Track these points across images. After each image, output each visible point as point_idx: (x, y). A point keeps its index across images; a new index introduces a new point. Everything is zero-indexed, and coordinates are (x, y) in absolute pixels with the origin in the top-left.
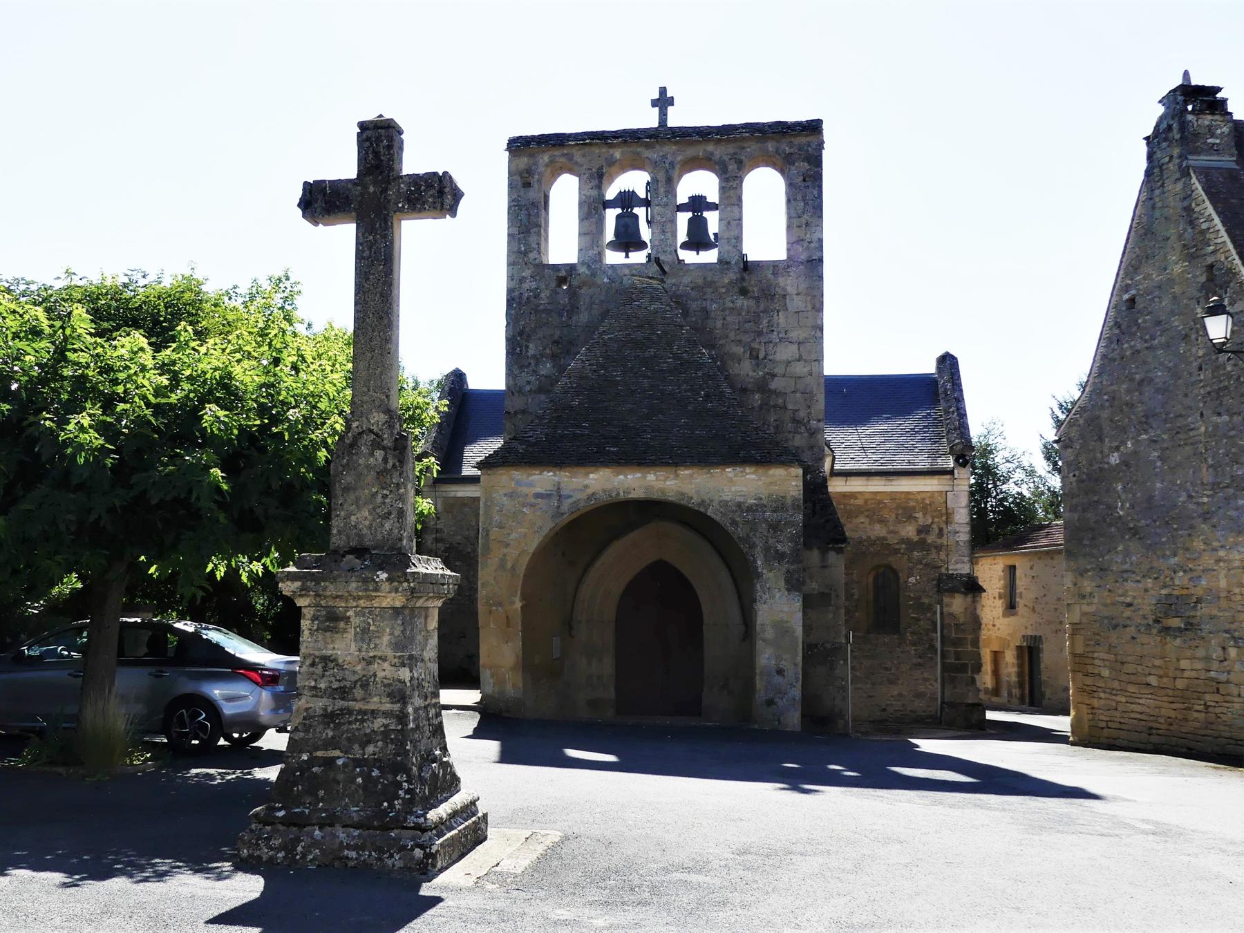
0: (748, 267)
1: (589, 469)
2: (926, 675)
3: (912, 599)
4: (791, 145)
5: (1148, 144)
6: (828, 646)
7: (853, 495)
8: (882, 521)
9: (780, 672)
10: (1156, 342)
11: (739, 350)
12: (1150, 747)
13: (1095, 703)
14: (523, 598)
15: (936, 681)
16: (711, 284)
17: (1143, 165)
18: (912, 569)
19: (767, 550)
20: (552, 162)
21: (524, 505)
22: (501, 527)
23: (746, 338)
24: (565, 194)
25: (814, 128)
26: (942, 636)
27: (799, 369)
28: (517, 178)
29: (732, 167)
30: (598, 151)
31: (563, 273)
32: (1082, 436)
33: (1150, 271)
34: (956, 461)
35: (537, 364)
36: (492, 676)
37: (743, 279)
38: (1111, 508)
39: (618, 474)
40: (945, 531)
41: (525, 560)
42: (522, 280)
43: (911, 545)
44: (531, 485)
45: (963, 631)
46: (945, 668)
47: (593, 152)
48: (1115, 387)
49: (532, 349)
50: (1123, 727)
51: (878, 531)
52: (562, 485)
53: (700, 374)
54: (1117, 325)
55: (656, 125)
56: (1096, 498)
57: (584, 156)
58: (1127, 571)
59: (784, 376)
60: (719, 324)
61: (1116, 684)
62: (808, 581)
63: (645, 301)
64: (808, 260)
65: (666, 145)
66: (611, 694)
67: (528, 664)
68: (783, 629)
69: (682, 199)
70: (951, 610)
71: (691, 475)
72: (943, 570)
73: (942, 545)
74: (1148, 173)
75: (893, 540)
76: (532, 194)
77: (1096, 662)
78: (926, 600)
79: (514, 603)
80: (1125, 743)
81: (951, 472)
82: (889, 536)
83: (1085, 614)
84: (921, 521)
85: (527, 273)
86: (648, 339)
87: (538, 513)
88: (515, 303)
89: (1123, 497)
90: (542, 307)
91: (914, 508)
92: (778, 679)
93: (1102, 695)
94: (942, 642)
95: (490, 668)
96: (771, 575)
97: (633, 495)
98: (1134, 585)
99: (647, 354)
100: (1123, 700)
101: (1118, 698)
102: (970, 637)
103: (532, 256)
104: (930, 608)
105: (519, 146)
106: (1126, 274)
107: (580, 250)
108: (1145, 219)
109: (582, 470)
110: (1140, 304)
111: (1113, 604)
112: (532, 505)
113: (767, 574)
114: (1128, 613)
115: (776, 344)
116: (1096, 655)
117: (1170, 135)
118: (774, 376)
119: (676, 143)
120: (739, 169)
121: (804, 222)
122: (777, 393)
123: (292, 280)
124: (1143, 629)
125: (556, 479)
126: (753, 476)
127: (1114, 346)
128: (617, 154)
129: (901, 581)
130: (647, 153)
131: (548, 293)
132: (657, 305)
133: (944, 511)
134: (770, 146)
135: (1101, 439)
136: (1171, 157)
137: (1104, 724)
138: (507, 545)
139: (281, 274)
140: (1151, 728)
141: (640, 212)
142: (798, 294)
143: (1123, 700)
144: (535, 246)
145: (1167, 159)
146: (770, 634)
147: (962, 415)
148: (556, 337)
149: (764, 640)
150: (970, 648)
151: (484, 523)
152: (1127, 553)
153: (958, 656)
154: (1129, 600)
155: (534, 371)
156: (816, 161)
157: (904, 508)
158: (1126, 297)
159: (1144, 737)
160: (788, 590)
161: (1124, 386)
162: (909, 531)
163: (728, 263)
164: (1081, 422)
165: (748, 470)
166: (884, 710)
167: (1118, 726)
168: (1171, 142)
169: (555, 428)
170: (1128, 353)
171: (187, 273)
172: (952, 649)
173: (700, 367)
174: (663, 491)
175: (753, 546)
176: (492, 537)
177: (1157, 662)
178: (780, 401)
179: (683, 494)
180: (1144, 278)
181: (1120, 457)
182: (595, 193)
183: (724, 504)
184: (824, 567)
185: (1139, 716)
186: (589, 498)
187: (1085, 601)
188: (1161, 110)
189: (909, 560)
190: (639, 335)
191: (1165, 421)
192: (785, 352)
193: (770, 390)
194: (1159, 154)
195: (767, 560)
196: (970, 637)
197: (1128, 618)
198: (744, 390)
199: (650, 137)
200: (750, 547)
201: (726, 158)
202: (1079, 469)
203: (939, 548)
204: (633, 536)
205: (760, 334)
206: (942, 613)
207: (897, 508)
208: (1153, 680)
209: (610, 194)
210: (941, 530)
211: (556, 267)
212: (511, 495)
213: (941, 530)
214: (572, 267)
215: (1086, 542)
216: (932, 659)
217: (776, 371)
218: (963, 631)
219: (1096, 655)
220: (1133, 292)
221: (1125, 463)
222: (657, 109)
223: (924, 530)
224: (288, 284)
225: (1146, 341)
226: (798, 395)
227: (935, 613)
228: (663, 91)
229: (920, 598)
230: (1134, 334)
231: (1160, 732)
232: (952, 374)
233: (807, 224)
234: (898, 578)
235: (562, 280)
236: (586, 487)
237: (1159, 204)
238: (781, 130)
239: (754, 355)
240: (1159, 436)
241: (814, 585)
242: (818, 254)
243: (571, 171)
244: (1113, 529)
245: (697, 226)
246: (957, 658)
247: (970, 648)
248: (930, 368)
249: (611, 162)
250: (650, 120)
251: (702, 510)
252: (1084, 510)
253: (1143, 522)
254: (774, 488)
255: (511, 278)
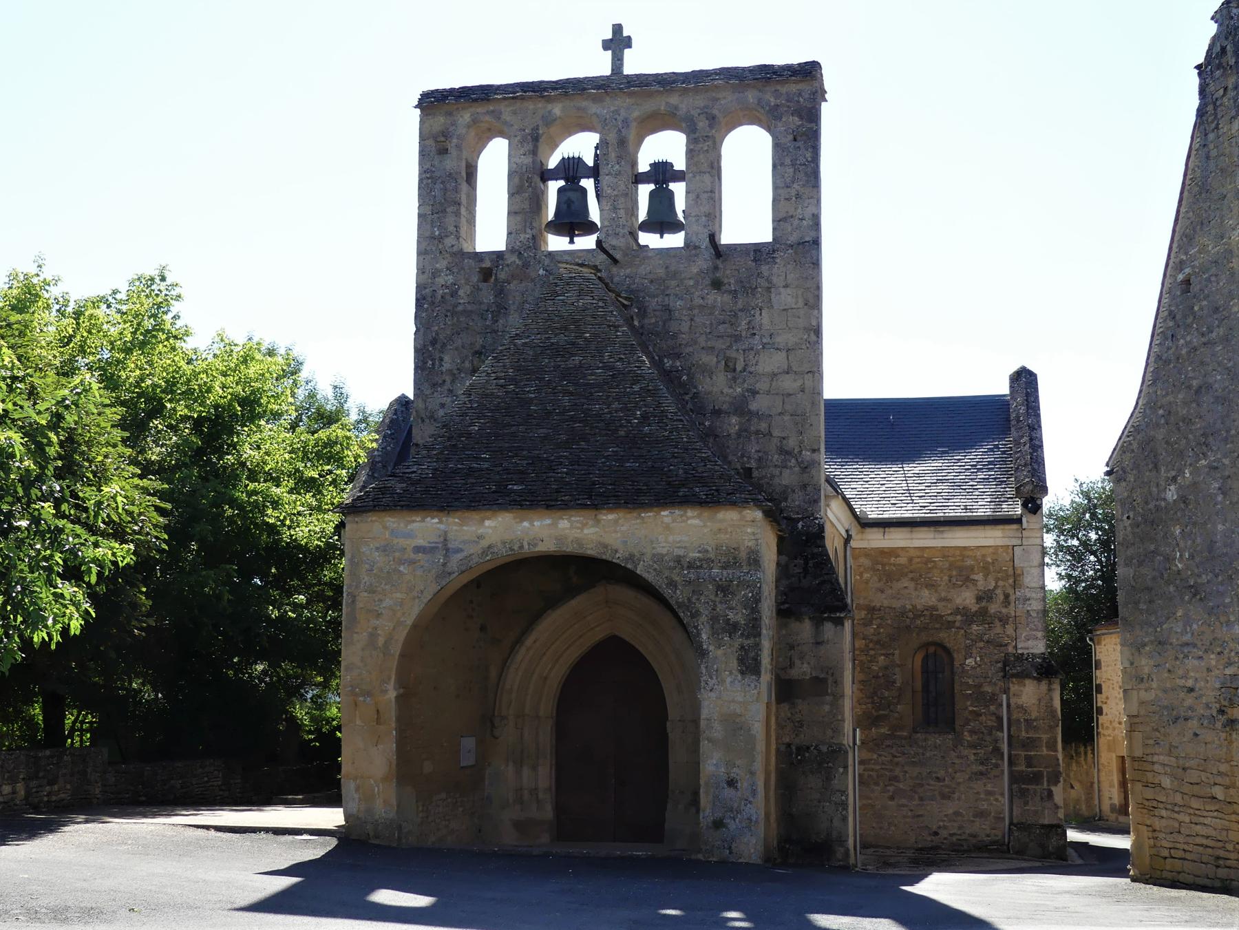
0: (720, 252)
1: (483, 514)
2: (989, 787)
3: (969, 687)
4: (777, 94)
5: (1199, 74)
6: (824, 749)
7: (893, 552)
8: (931, 586)
9: (731, 783)
10: (1214, 335)
11: (709, 359)
12: (1218, 884)
13: (1157, 824)
14: (401, 682)
15: (1002, 794)
16: (674, 275)
17: (1195, 102)
18: (968, 647)
19: (714, 619)
20: (475, 121)
21: (401, 562)
22: (372, 591)
23: (720, 345)
24: (494, 162)
25: (809, 72)
26: (1010, 736)
27: (788, 384)
28: (430, 142)
29: (702, 124)
30: (534, 106)
31: (487, 264)
32: (1136, 466)
33: (1205, 240)
34: (1024, 505)
35: (453, 381)
36: (357, 790)
37: (716, 268)
38: (1169, 559)
39: (522, 521)
40: (1012, 598)
41: (402, 635)
42: (435, 274)
43: (969, 617)
44: (409, 535)
45: (1036, 729)
46: (1015, 778)
47: (528, 108)
48: (1170, 398)
49: (448, 362)
50: (1188, 856)
51: (926, 598)
52: (450, 536)
53: (636, 388)
54: (1172, 315)
55: (607, 71)
56: (1152, 547)
57: (515, 113)
58: (1187, 644)
59: (768, 393)
60: (685, 327)
61: (1178, 798)
62: (798, 662)
63: (571, 296)
64: (797, 241)
65: (625, 98)
66: (548, 813)
67: (406, 769)
68: (735, 725)
69: (643, 167)
70: (1020, 702)
71: (616, 521)
72: (1010, 649)
73: (1008, 617)
74: (1201, 113)
75: (945, 610)
76: (450, 163)
77: (1156, 767)
78: (988, 689)
79: (386, 691)
80: (1190, 879)
81: (1018, 521)
82: (940, 605)
83: (1142, 703)
84: (981, 585)
85: (441, 265)
86: (573, 344)
87: (419, 572)
88: (425, 301)
89: (1182, 544)
90: (460, 308)
91: (972, 569)
92: (728, 792)
93: (1164, 813)
94: (1010, 745)
95: (355, 779)
96: (720, 652)
97: (542, 548)
98: (1196, 662)
99: (570, 364)
100: (1187, 819)
101: (1182, 817)
102: (1045, 737)
103: (449, 241)
104: (993, 699)
105: (432, 102)
106: (1180, 247)
107: (509, 234)
108: (1198, 173)
109: (476, 516)
110: (1195, 288)
111: (1173, 689)
112: (412, 562)
113: (714, 652)
114: (1189, 702)
115: (757, 353)
116: (1155, 758)
117: (1224, 60)
118: (754, 393)
119: (631, 94)
120: (711, 126)
121: (793, 192)
122: (758, 415)
123: (169, 282)
124: (1205, 723)
125: (442, 527)
126: (696, 522)
127: (1168, 343)
128: (557, 109)
129: (957, 664)
130: (594, 108)
131: (468, 289)
132: (588, 300)
133: (1011, 571)
134: (751, 96)
135: (1156, 468)
136: (1226, 89)
137: (1165, 853)
138: (379, 615)
139: (155, 273)
140: (1218, 858)
141: (588, 184)
142: (786, 286)
143: (1187, 819)
144: (451, 228)
145: (1221, 92)
146: (717, 731)
147: (1036, 446)
148: (478, 347)
149: (709, 740)
150: (1045, 751)
151: (350, 586)
152: (1187, 622)
153: (1029, 761)
154: (1190, 683)
155: (450, 391)
156: (812, 116)
157: (961, 569)
158: (1181, 277)
159: (1210, 870)
160: (742, 673)
161: (1180, 396)
162: (966, 598)
163: (696, 247)
164: (1135, 446)
165: (690, 513)
166: (936, 834)
167: (1180, 854)
168: (1225, 69)
169: (447, 460)
170: (1184, 351)
171: (33, 270)
172: (1023, 754)
173: (637, 379)
174: (578, 541)
175: (696, 615)
176: (360, 605)
177: (1224, 768)
178: (763, 426)
179: (606, 546)
180: (1200, 252)
181: (1177, 490)
182: (528, 160)
183: (658, 558)
184: (818, 643)
185: (1205, 842)
186: (484, 552)
187: (1142, 686)
188: (1213, 28)
189: (966, 635)
190: (562, 339)
191: (1226, 440)
192: (770, 362)
193: (750, 412)
194: (1212, 88)
195: (714, 633)
196: (1045, 737)
197: (1190, 708)
198: (717, 413)
199: (598, 87)
200: (693, 616)
201: (695, 113)
202: (1134, 509)
203: (1004, 620)
204: (575, 603)
205: (737, 338)
206: (1009, 706)
207: (952, 566)
208: (1218, 792)
209: (553, 163)
210: (1007, 596)
211: (479, 257)
212: (385, 549)
213: (1007, 596)
214: (499, 255)
215: (1143, 606)
216: (997, 766)
217: (758, 386)
218: (1036, 729)
219: (1155, 758)
220: (1187, 270)
221: (1184, 499)
222: (610, 52)
223: (984, 597)
224: (163, 286)
225: (1203, 335)
226: (786, 418)
227: (1001, 705)
228: (618, 29)
229: (980, 686)
230: (1190, 326)
231: (1229, 863)
232: (1027, 395)
233: (798, 196)
234: (952, 660)
235: (486, 274)
236: (480, 537)
237: (1214, 153)
238: (766, 75)
239: (730, 367)
240: (1219, 460)
241: (806, 667)
242: (813, 234)
243: (502, 134)
244: (1172, 589)
245: (662, 199)
246: (1029, 765)
247: (1045, 751)
248: (1002, 388)
249: (549, 121)
250: (600, 65)
251: (629, 566)
252: (1141, 564)
253: (1204, 578)
254: (723, 537)
255: (421, 270)
